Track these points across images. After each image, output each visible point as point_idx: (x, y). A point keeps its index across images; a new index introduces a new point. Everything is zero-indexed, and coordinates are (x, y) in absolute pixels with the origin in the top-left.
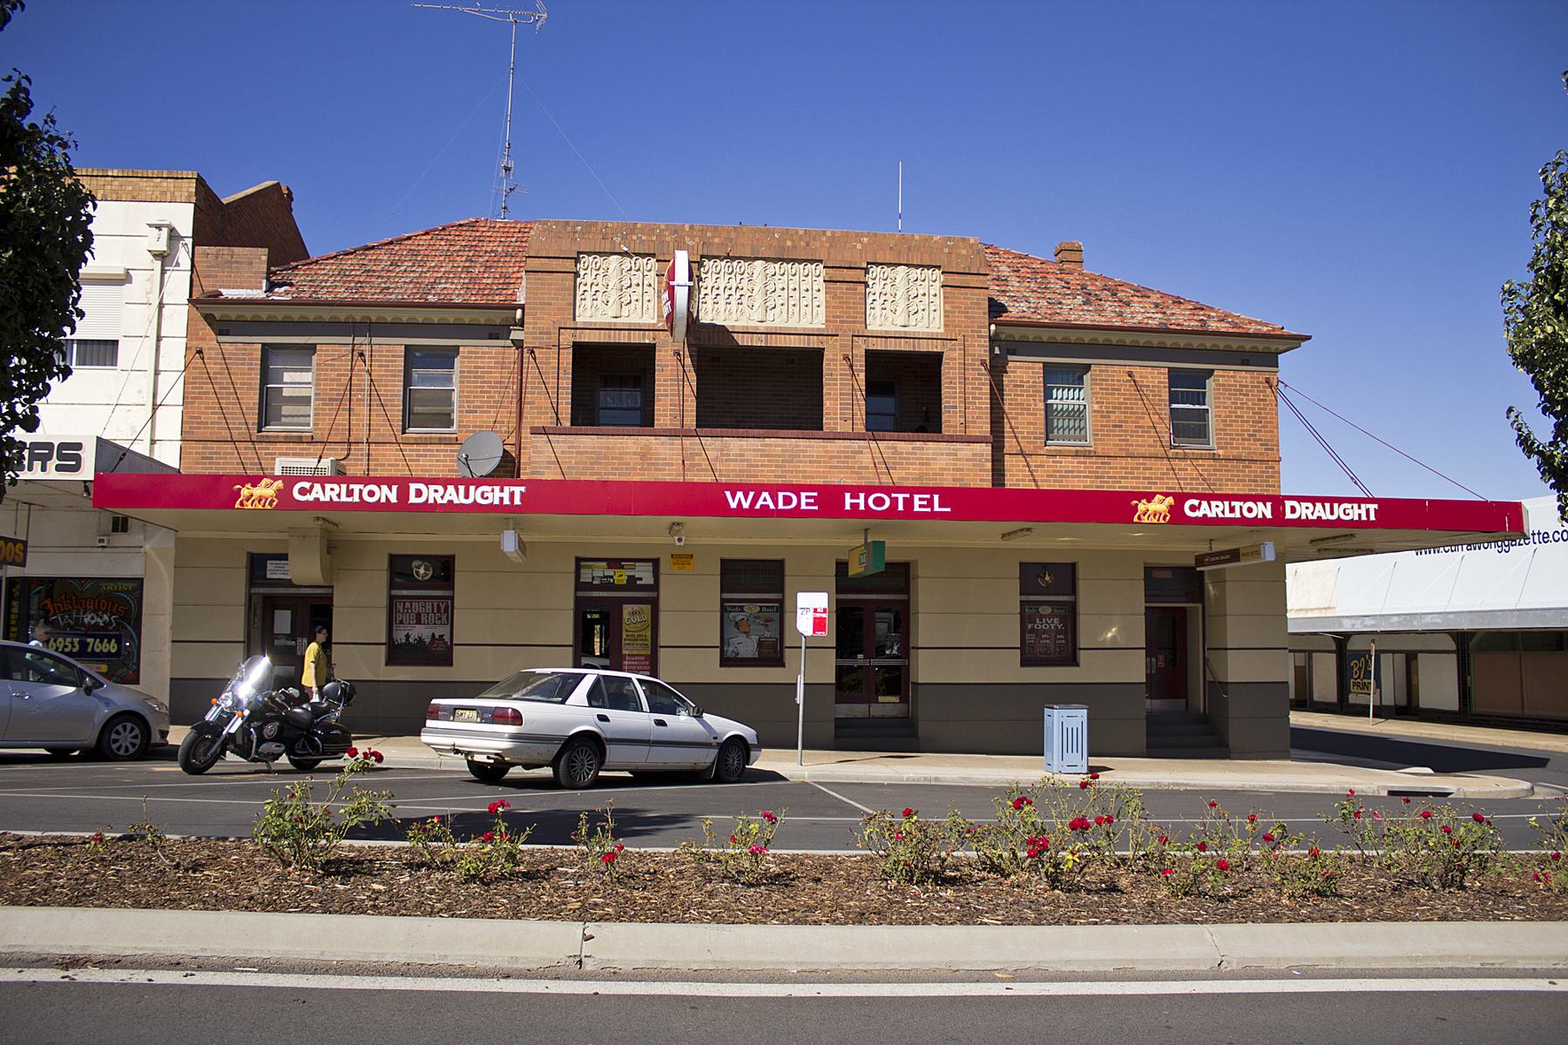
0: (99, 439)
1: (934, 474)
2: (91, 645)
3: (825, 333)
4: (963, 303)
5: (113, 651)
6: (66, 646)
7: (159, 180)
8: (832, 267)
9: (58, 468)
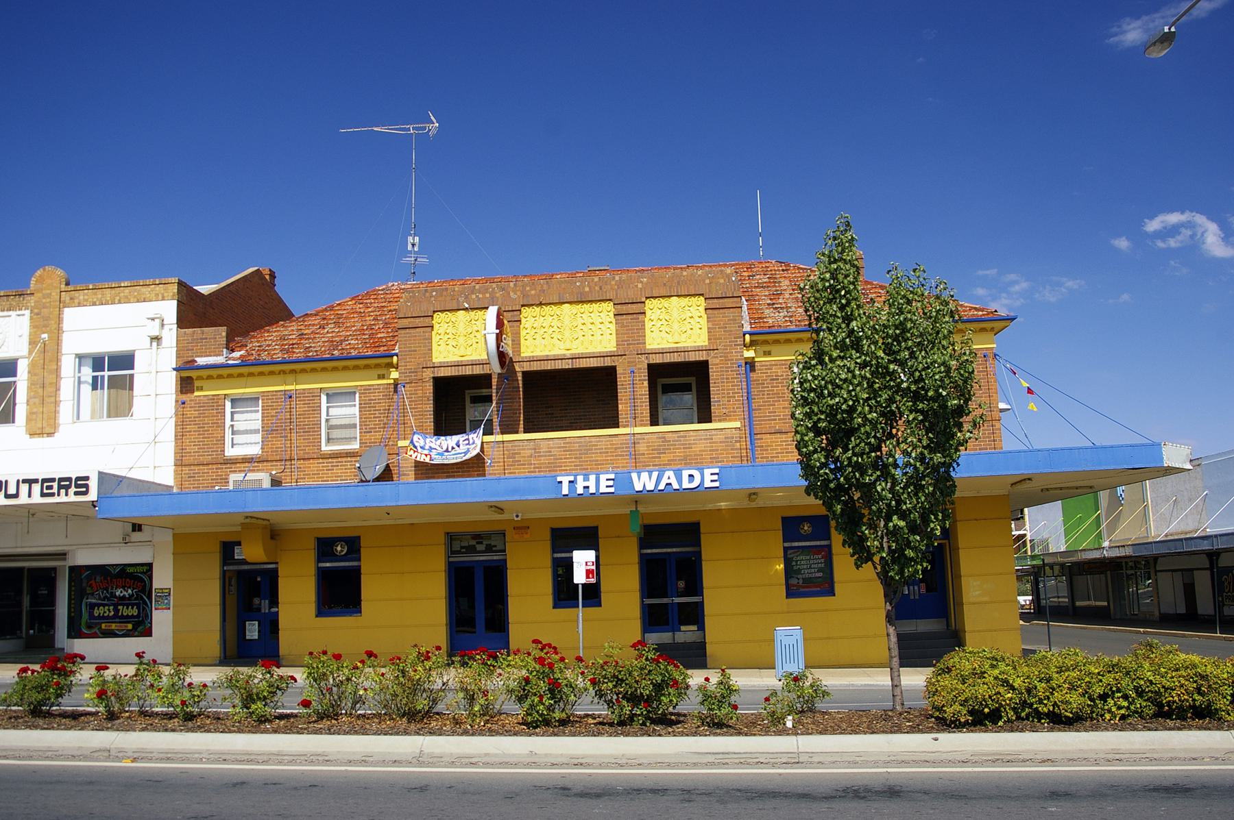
0: (100, 473)
1: (695, 455)
2: (121, 611)
3: (616, 354)
4: (721, 320)
5: (135, 614)
6: (105, 612)
7: (153, 286)
8: (619, 304)
9: (76, 493)
